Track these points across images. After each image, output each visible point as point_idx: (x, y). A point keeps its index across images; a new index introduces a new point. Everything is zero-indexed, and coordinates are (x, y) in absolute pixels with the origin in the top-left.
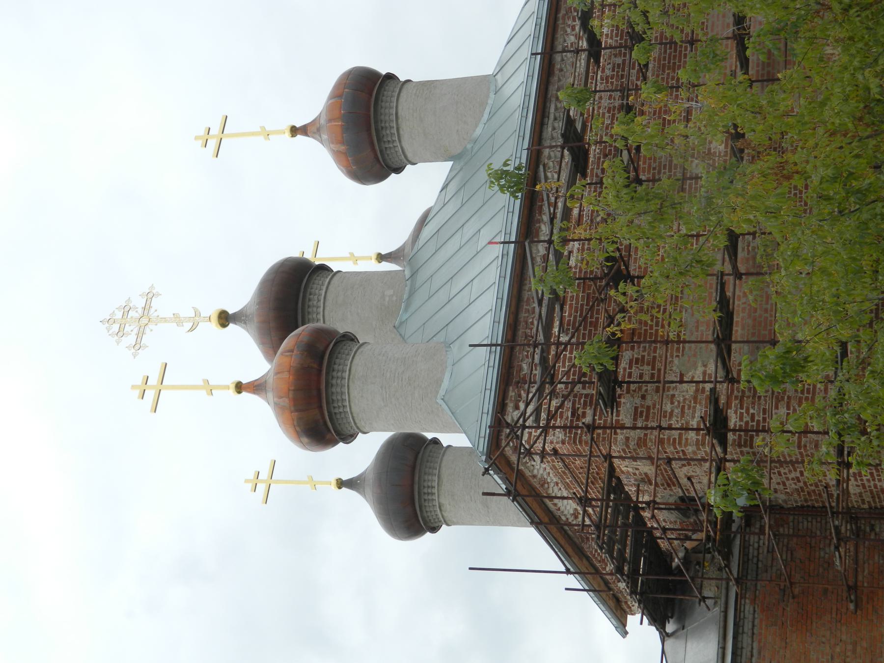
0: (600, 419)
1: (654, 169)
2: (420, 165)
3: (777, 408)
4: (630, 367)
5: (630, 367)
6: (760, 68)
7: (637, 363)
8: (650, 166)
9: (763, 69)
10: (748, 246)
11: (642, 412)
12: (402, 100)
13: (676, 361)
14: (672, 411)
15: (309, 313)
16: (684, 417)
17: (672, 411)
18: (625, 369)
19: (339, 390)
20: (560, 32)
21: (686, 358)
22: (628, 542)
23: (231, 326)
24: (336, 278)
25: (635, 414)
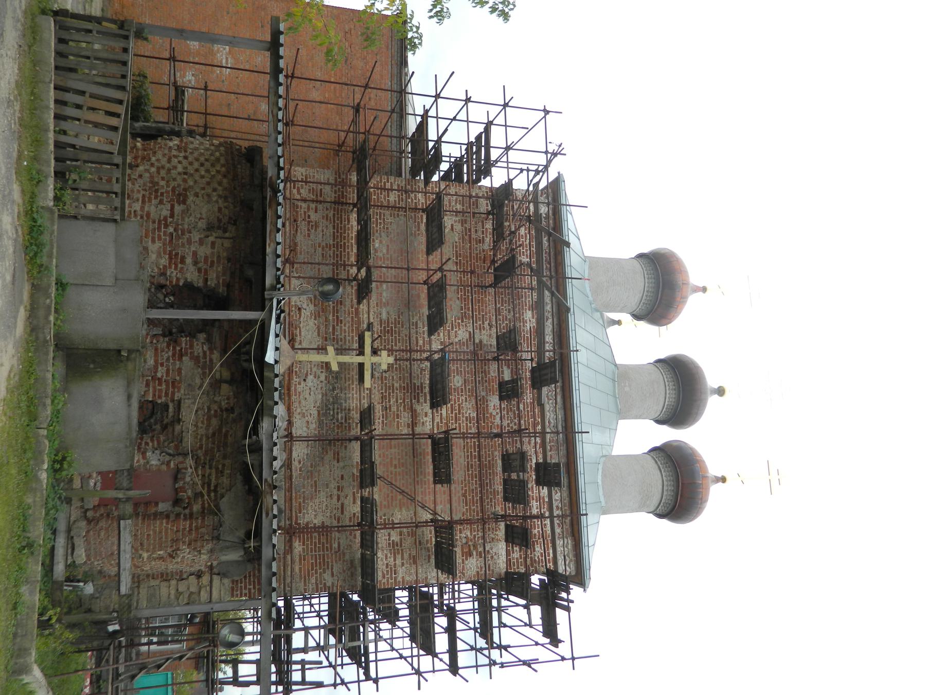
0: (474, 442)
1: (486, 381)
2: (645, 363)
3: (395, 201)
4: (483, 237)
5: (483, 237)
6: (423, 460)
7: (480, 240)
8: (489, 383)
9: (421, 460)
10: (420, 317)
11: (473, 205)
12: (660, 481)
13: (457, 239)
14: (456, 203)
15: (674, 385)
16: (434, 364)
17: (456, 203)
18: (487, 237)
19: (650, 281)
20: (567, 501)
21: (451, 241)
22: (465, 176)
23: (716, 387)
24: (652, 510)
25: (477, 204)
